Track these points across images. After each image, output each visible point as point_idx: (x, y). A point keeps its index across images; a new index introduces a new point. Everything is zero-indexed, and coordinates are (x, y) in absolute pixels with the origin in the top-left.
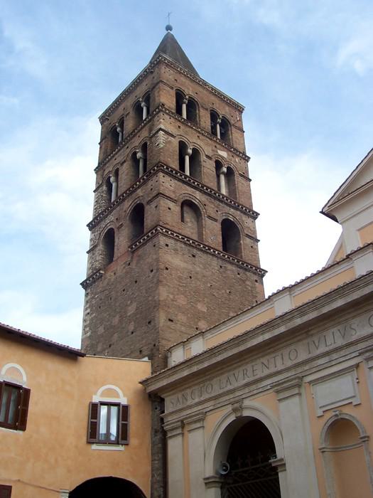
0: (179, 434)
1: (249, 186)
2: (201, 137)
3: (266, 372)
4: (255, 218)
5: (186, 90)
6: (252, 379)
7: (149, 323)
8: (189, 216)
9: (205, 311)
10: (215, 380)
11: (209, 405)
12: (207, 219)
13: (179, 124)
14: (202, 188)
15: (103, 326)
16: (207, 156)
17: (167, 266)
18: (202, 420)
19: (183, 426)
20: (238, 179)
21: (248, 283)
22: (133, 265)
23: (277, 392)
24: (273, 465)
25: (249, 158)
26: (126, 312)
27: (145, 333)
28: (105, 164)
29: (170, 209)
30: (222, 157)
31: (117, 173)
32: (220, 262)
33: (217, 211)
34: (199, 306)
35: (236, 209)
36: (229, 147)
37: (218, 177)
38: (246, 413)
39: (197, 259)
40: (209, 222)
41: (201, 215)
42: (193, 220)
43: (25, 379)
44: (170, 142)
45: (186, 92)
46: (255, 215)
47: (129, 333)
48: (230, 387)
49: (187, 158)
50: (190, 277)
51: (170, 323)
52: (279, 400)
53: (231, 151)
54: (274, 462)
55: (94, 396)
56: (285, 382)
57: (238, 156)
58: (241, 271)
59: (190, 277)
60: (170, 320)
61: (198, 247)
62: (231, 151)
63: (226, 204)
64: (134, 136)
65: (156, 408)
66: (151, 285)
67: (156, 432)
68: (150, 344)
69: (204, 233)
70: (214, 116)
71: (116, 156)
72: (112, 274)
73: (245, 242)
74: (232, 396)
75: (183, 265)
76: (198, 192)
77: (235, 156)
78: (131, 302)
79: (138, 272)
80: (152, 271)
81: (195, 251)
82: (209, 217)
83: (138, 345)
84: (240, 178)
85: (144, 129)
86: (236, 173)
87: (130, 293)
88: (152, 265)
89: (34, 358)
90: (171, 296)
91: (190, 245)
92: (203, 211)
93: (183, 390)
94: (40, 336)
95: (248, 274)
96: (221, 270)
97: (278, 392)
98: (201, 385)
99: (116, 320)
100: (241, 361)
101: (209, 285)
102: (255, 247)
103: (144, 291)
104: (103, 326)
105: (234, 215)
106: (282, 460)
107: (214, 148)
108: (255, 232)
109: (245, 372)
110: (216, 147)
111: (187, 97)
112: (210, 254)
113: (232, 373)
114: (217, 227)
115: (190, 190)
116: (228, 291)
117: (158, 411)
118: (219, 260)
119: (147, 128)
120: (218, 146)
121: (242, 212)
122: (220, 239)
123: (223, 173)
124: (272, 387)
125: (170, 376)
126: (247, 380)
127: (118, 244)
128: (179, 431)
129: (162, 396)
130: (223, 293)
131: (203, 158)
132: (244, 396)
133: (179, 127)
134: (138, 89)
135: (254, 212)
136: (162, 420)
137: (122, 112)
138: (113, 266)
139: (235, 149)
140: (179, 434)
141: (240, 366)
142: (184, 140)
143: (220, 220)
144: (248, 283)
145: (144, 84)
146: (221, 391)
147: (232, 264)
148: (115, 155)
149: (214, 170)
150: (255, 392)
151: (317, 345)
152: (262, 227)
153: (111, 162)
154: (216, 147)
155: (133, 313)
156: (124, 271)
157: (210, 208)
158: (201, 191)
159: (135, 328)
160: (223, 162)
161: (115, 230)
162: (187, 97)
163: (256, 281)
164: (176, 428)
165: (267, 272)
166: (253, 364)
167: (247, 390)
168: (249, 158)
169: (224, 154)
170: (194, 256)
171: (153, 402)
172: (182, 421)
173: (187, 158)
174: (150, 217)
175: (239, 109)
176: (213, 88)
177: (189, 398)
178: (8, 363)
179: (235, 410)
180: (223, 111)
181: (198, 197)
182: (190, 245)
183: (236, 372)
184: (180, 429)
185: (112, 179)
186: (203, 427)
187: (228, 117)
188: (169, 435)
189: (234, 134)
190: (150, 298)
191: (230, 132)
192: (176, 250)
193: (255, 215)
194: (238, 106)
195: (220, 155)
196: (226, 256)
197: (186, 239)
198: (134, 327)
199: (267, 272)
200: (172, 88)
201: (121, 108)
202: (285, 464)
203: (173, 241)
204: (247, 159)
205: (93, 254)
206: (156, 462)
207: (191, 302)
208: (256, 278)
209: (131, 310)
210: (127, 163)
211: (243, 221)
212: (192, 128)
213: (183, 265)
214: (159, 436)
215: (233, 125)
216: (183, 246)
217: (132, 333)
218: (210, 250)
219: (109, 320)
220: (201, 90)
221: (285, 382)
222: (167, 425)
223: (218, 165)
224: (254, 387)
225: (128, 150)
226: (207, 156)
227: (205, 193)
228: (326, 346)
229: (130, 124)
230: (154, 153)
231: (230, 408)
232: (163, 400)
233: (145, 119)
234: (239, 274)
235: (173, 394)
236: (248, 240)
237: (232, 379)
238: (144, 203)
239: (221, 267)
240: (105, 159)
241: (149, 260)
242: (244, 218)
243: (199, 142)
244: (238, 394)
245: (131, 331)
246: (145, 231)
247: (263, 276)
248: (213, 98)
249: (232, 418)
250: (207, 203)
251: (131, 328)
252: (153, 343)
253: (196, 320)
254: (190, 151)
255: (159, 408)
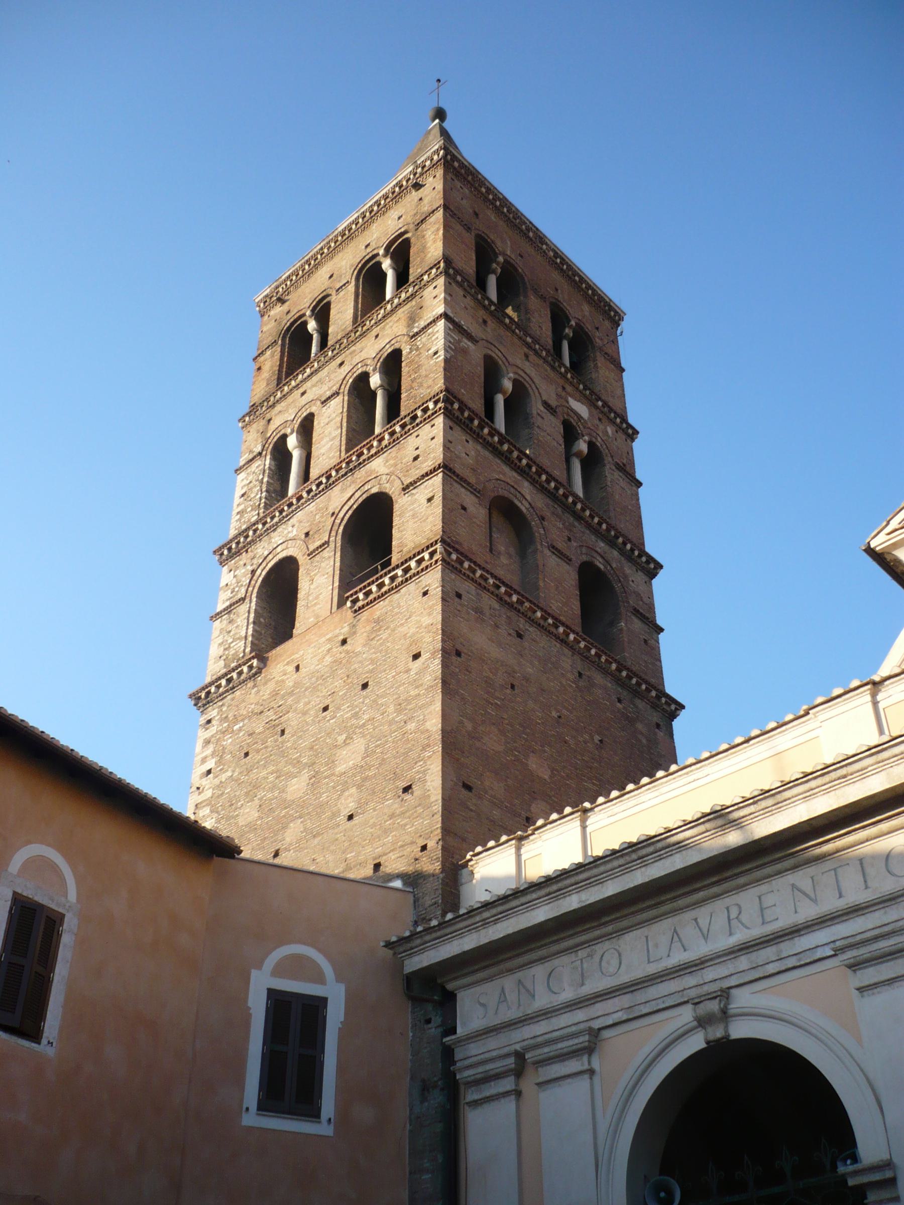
0: (506, 1094)
1: (636, 497)
2: (532, 357)
3: (808, 912)
4: (652, 575)
5: (499, 243)
6: (757, 932)
7: (407, 789)
8: (504, 542)
9: (546, 777)
10: (629, 937)
11: (613, 1009)
12: (547, 552)
13: (482, 313)
14: (530, 472)
15: (257, 801)
16: (546, 404)
17: (459, 647)
18: (589, 1050)
19: (518, 1072)
20: (611, 475)
21: (639, 726)
22: (357, 644)
23: (850, 967)
24: (851, 1182)
25: (636, 432)
26: (331, 763)
27: (392, 816)
28: (273, 406)
29: (464, 508)
30: (579, 417)
31: (306, 428)
32: (580, 665)
33: (569, 539)
34: (533, 763)
35: (612, 543)
36: (592, 398)
37: (568, 461)
38: (740, 1030)
39: (526, 644)
40: (552, 561)
41: (532, 540)
42: (512, 550)
43: (72, 896)
44: (465, 351)
45: (499, 245)
46: (652, 568)
47: (342, 818)
48: (679, 957)
49: (500, 400)
50: (513, 687)
51: (464, 792)
52: (861, 990)
53: (597, 407)
54: (856, 1173)
55: (254, 973)
56: (876, 938)
57: (612, 422)
58: (624, 694)
59: (513, 687)
60: (468, 787)
61: (529, 614)
62: (597, 407)
63: (589, 526)
64: (363, 335)
65: (428, 1021)
66: (413, 693)
67: (425, 1088)
68: (412, 843)
69: (541, 584)
70: (558, 318)
71: (308, 384)
72: (291, 668)
73: (630, 626)
74: (690, 981)
75: (495, 652)
76: (526, 484)
77: (604, 420)
78: (349, 737)
79: (372, 661)
80: (416, 657)
81: (522, 624)
82: (553, 548)
83: (369, 849)
84: (617, 474)
85: (394, 318)
86: (608, 459)
87: (345, 713)
88: (415, 642)
89: (104, 831)
90: (469, 726)
91: (511, 606)
92: (539, 532)
93: (521, 967)
94: (132, 783)
95: (640, 704)
96: (581, 683)
97: (855, 966)
98: (582, 954)
99: (297, 786)
100: (726, 879)
101: (554, 714)
102: (652, 642)
103: (392, 708)
104: (257, 801)
105: (607, 557)
106: (888, 1165)
107: (560, 389)
108: (651, 607)
109: (734, 913)
110: (564, 388)
111: (573, 323)
112: (557, 637)
113: (688, 915)
114: (569, 577)
115: (511, 475)
116: (597, 738)
117: (433, 1030)
118: (576, 657)
119: (402, 313)
120: (569, 389)
121: (622, 551)
122: (576, 606)
123: (578, 454)
124: (837, 952)
125: (485, 923)
126: (740, 936)
127: (308, 595)
128: (508, 1084)
129: (450, 986)
130: (585, 742)
131: (536, 407)
132: (733, 981)
133: (485, 322)
134: (374, 227)
135: (651, 559)
136: (448, 1054)
137: (327, 283)
138: (282, 659)
139: (605, 404)
140: (506, 1094)
141: (717, 896)
142: (495, 354)
143: (577, 561)
144: (639, 726)
145: (393, 214)
146: (652, 969)
147: (605, 672)
148: (304, 381)
149: (562, 441)
150: (772, 968)
151: (812, 895)
152: (667, 596)
153: (290, 399)
154: (564, 388)
155: (355, 767)
156: (328, 659)
157: (553, 528)
158: (534, 482)
159: (362, 804)
160: (580, 429)
161: (302, 560)
162: (501, 259)
163: (658, 726)
164: (497, 1076)
165: (683, 707)
166: (764, 888)
167: (743, 962)
168: (636, 432)
169: (582, 410)
170: (520, 636)
171: (416, 1000)
172: (520, 1056)
173: (500, 400)
174: (411, 525)
175: (612, 315)
176: (557, 254)
177: (540, 989)
178: (29, 842)
179: (702, 1022)
180: (579, 312)
181: (527, 497)
182: (511, 606)
183: (703, 914)
184: (512, 1079)
185: (292, 442)
186: (591, 1072)
187: (589, 327)
188: (472, 1095)
189: (601, 372)
190: (411, 726)
191: (591, 364)
192: (479, 611)
193: (652, 568)
194: (611, 308)
195: (572, 410)
196: (593, 652)
197: (503, 589)
198: (359, 802)
199: (683, 707)
200: (468, 229)
201: (323, 272)
202: (892, 1182)
203: (472, 588)
204: (631, 433)
205: (231, 622)
206: (426, 1176)
207: (515, 749)
208: (655, 717)
209: (349, 758)
210: (340, 398)
211: (626, 577)
212: (513, 332)
213: (495, 652)
214: (437, 1098)
215: (601, 349)
216: (496, 605)
217: (351, 817)
218: (557, 627)
219: (273, 788)
220: (531, 250)
221: (876, 938)
222: (468, 1067)
223: (570, 433)
224: (769, 953)
225: (346, 368)
226: (546, 404)
227: (543, 489)
228: (649, 962)
229: (343, 313)
230: (423, 372)
231: (686, 1015)
232: (449, 999)
233: (392, 299)
234: (619, 701)
235: (490, 979)
236: (637, 625)
237: (689, 932)
238: (393, 489)
239: (580, 675)
240: (273, 394)
241: (410, 629)
242: (628, 569)
243: (527, 367)
244: (710, 974)
245: (346, 812)
246: (395, 558)
247: (673, 716)
248: (555, 276)
249: (696, 1043)
250: (548, 514)
251: (348, 804)
252: (421, 843)
253: (527, 797)
254: (508, 385)
255: (437, 1020)
